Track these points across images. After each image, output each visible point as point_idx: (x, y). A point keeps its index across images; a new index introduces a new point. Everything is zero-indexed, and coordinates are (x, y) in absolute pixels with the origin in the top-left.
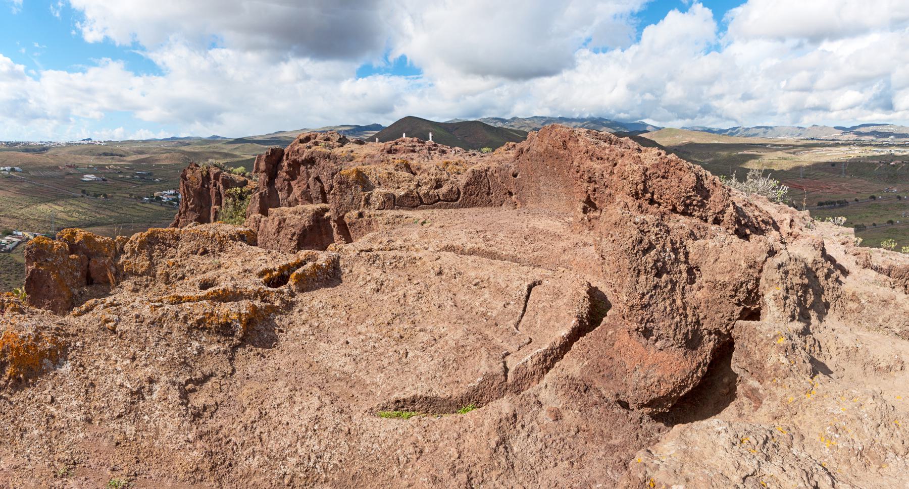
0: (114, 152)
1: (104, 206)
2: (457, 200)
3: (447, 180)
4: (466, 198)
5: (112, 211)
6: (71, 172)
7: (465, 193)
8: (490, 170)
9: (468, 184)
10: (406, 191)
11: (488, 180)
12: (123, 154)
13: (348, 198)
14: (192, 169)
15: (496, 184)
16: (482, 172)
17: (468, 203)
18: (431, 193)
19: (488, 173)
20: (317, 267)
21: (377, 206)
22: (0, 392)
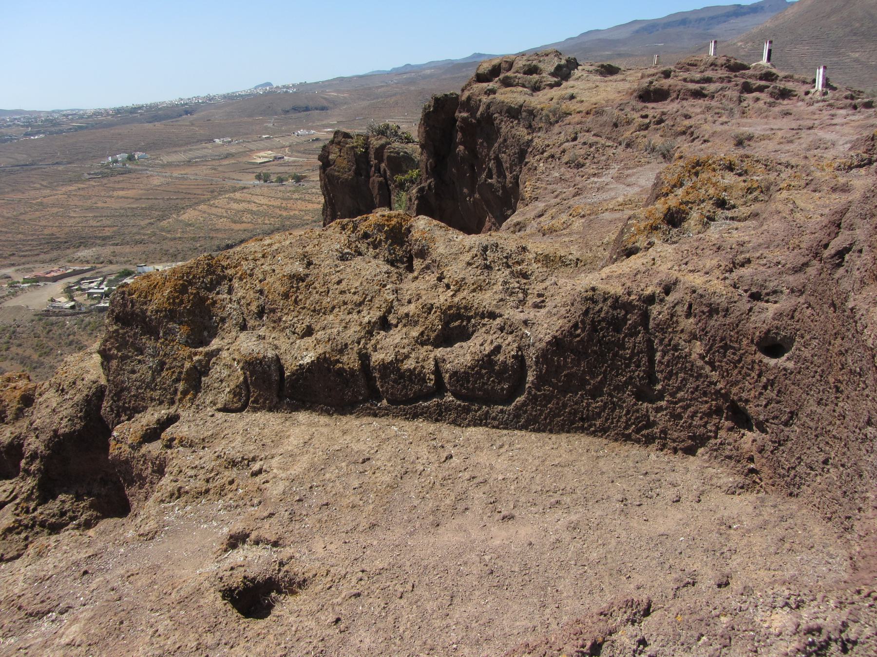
0: (311, 104)
1: (296, 196)
2: (508, 401)
3: (493, 316)
4: (548, 399)
5: (309, 201)
6: (233, 151)
7: (541, 380)
8: (671, 299)
9: (558, 344)
10: (320, 350)
11: (650, 342)
12: (325, 104)
13: (144, 369)
14: (339, 143)
15: (680, 359)
16: (628, 307)
17: (554, 415)
18: (409, 364)
19: (655, 309)
20: (554, 353)
21: (223, 398)
22: (874, 192)
